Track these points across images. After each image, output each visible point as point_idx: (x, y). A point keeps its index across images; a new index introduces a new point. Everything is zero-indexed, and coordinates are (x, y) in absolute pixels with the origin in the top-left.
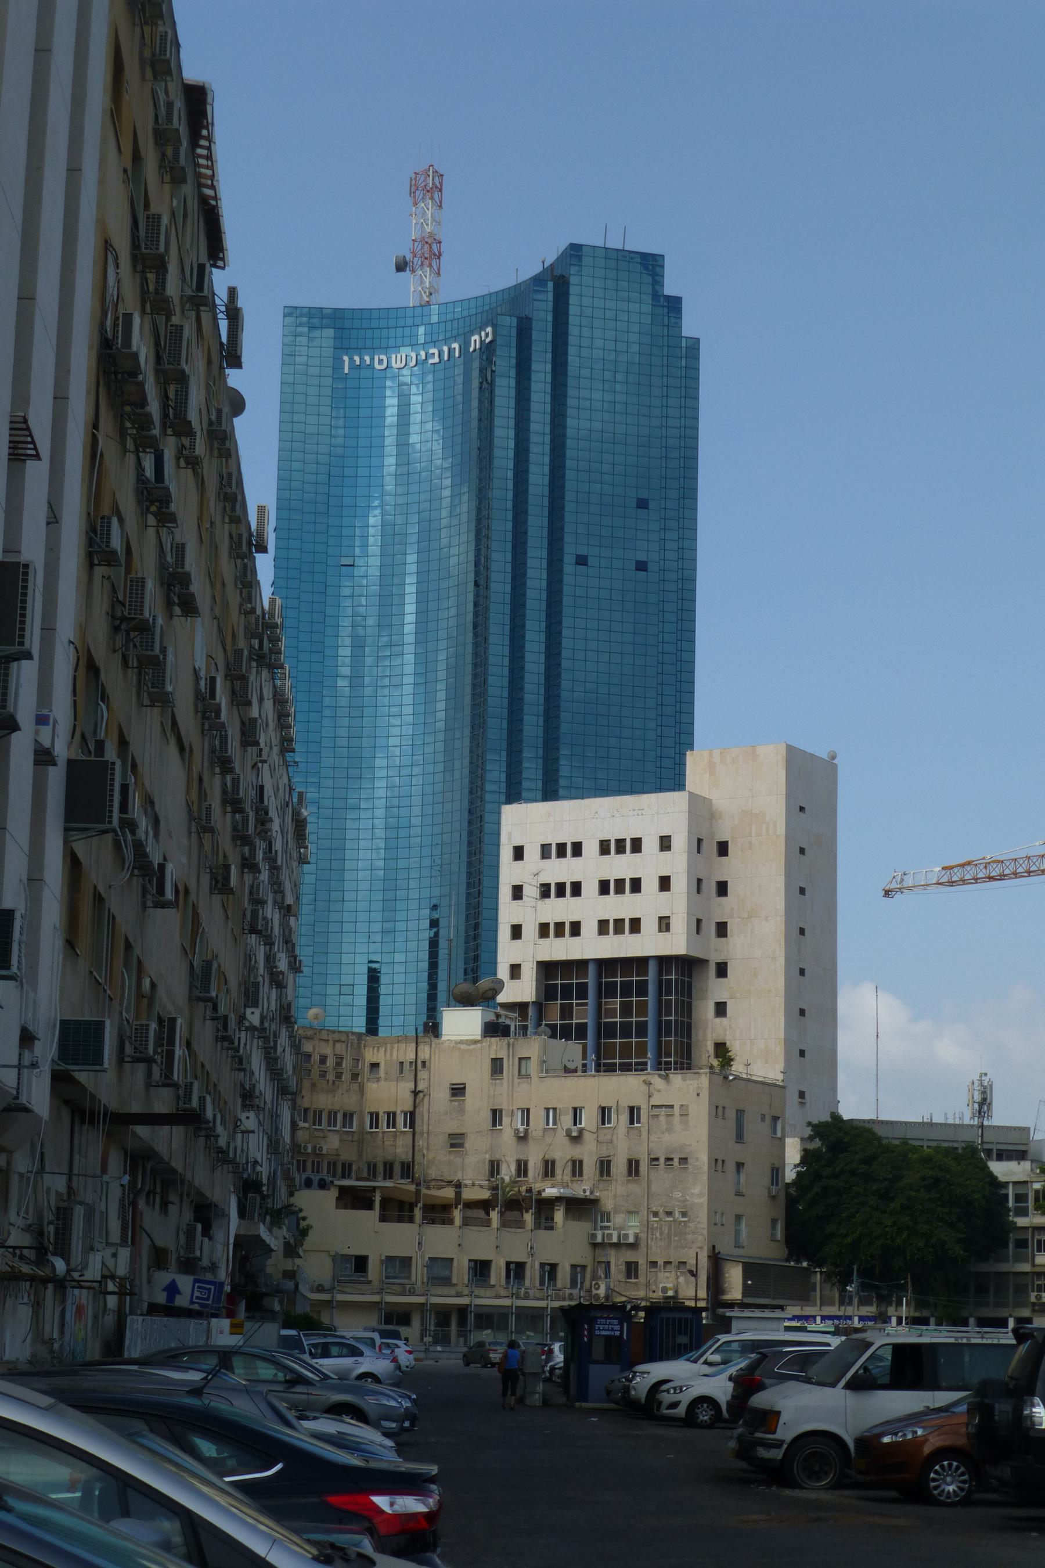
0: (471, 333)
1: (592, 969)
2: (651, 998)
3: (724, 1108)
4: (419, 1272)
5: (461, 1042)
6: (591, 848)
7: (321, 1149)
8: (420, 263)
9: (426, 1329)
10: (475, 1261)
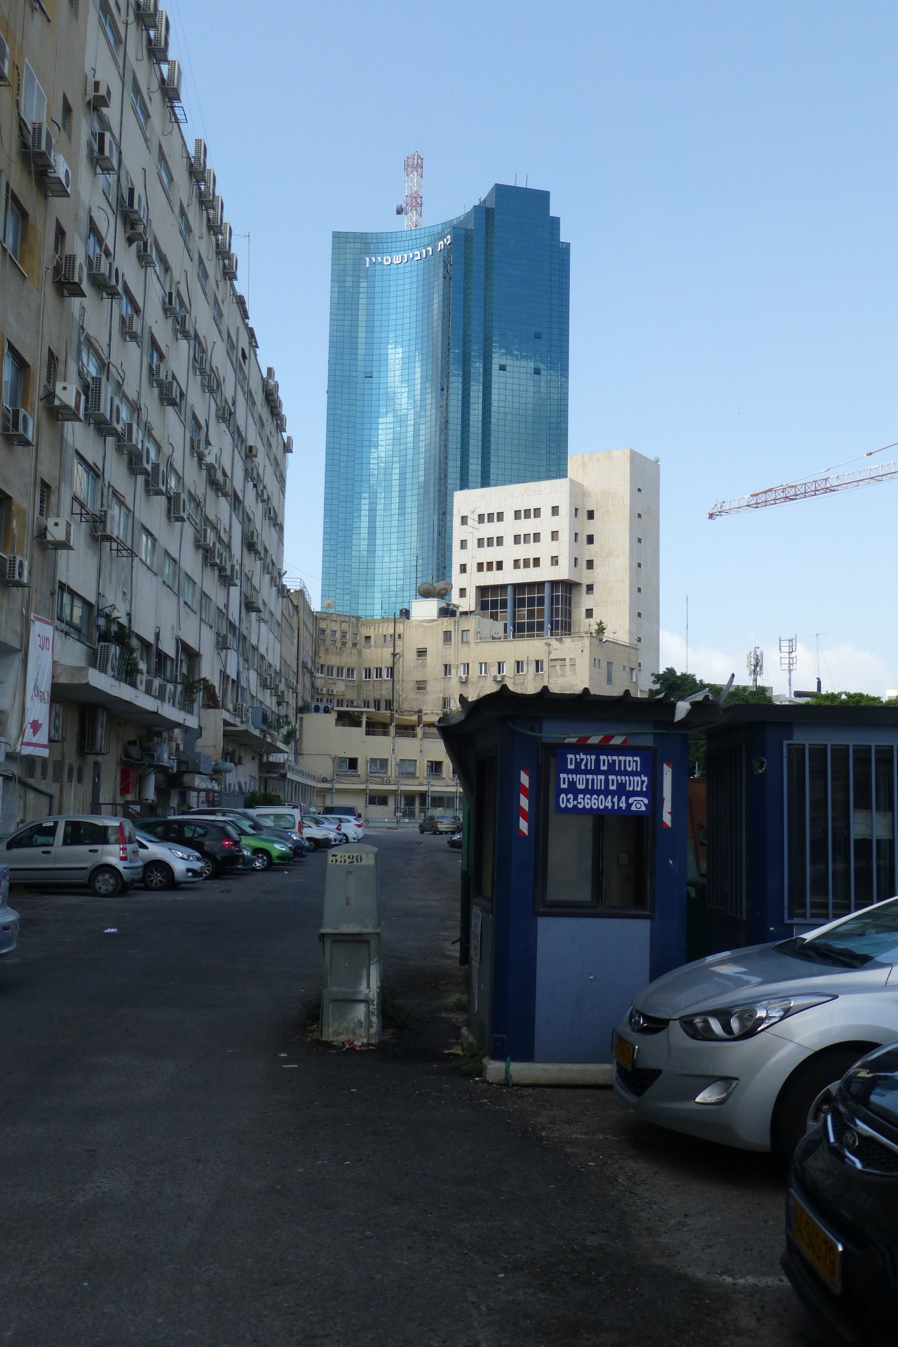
0: (440, 239)
1: (510, 590)
2: (547, 607)
3: (599, 660)
4: (393, 768)
5: (424, 621)
6: (509, 516)
7: (332, 691)
8: (410, 209)
9: (398, 808)
10: (432, 762)
